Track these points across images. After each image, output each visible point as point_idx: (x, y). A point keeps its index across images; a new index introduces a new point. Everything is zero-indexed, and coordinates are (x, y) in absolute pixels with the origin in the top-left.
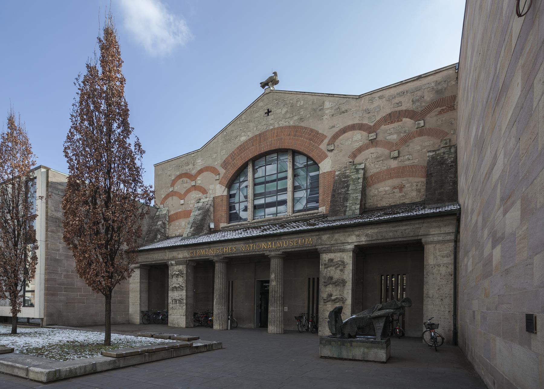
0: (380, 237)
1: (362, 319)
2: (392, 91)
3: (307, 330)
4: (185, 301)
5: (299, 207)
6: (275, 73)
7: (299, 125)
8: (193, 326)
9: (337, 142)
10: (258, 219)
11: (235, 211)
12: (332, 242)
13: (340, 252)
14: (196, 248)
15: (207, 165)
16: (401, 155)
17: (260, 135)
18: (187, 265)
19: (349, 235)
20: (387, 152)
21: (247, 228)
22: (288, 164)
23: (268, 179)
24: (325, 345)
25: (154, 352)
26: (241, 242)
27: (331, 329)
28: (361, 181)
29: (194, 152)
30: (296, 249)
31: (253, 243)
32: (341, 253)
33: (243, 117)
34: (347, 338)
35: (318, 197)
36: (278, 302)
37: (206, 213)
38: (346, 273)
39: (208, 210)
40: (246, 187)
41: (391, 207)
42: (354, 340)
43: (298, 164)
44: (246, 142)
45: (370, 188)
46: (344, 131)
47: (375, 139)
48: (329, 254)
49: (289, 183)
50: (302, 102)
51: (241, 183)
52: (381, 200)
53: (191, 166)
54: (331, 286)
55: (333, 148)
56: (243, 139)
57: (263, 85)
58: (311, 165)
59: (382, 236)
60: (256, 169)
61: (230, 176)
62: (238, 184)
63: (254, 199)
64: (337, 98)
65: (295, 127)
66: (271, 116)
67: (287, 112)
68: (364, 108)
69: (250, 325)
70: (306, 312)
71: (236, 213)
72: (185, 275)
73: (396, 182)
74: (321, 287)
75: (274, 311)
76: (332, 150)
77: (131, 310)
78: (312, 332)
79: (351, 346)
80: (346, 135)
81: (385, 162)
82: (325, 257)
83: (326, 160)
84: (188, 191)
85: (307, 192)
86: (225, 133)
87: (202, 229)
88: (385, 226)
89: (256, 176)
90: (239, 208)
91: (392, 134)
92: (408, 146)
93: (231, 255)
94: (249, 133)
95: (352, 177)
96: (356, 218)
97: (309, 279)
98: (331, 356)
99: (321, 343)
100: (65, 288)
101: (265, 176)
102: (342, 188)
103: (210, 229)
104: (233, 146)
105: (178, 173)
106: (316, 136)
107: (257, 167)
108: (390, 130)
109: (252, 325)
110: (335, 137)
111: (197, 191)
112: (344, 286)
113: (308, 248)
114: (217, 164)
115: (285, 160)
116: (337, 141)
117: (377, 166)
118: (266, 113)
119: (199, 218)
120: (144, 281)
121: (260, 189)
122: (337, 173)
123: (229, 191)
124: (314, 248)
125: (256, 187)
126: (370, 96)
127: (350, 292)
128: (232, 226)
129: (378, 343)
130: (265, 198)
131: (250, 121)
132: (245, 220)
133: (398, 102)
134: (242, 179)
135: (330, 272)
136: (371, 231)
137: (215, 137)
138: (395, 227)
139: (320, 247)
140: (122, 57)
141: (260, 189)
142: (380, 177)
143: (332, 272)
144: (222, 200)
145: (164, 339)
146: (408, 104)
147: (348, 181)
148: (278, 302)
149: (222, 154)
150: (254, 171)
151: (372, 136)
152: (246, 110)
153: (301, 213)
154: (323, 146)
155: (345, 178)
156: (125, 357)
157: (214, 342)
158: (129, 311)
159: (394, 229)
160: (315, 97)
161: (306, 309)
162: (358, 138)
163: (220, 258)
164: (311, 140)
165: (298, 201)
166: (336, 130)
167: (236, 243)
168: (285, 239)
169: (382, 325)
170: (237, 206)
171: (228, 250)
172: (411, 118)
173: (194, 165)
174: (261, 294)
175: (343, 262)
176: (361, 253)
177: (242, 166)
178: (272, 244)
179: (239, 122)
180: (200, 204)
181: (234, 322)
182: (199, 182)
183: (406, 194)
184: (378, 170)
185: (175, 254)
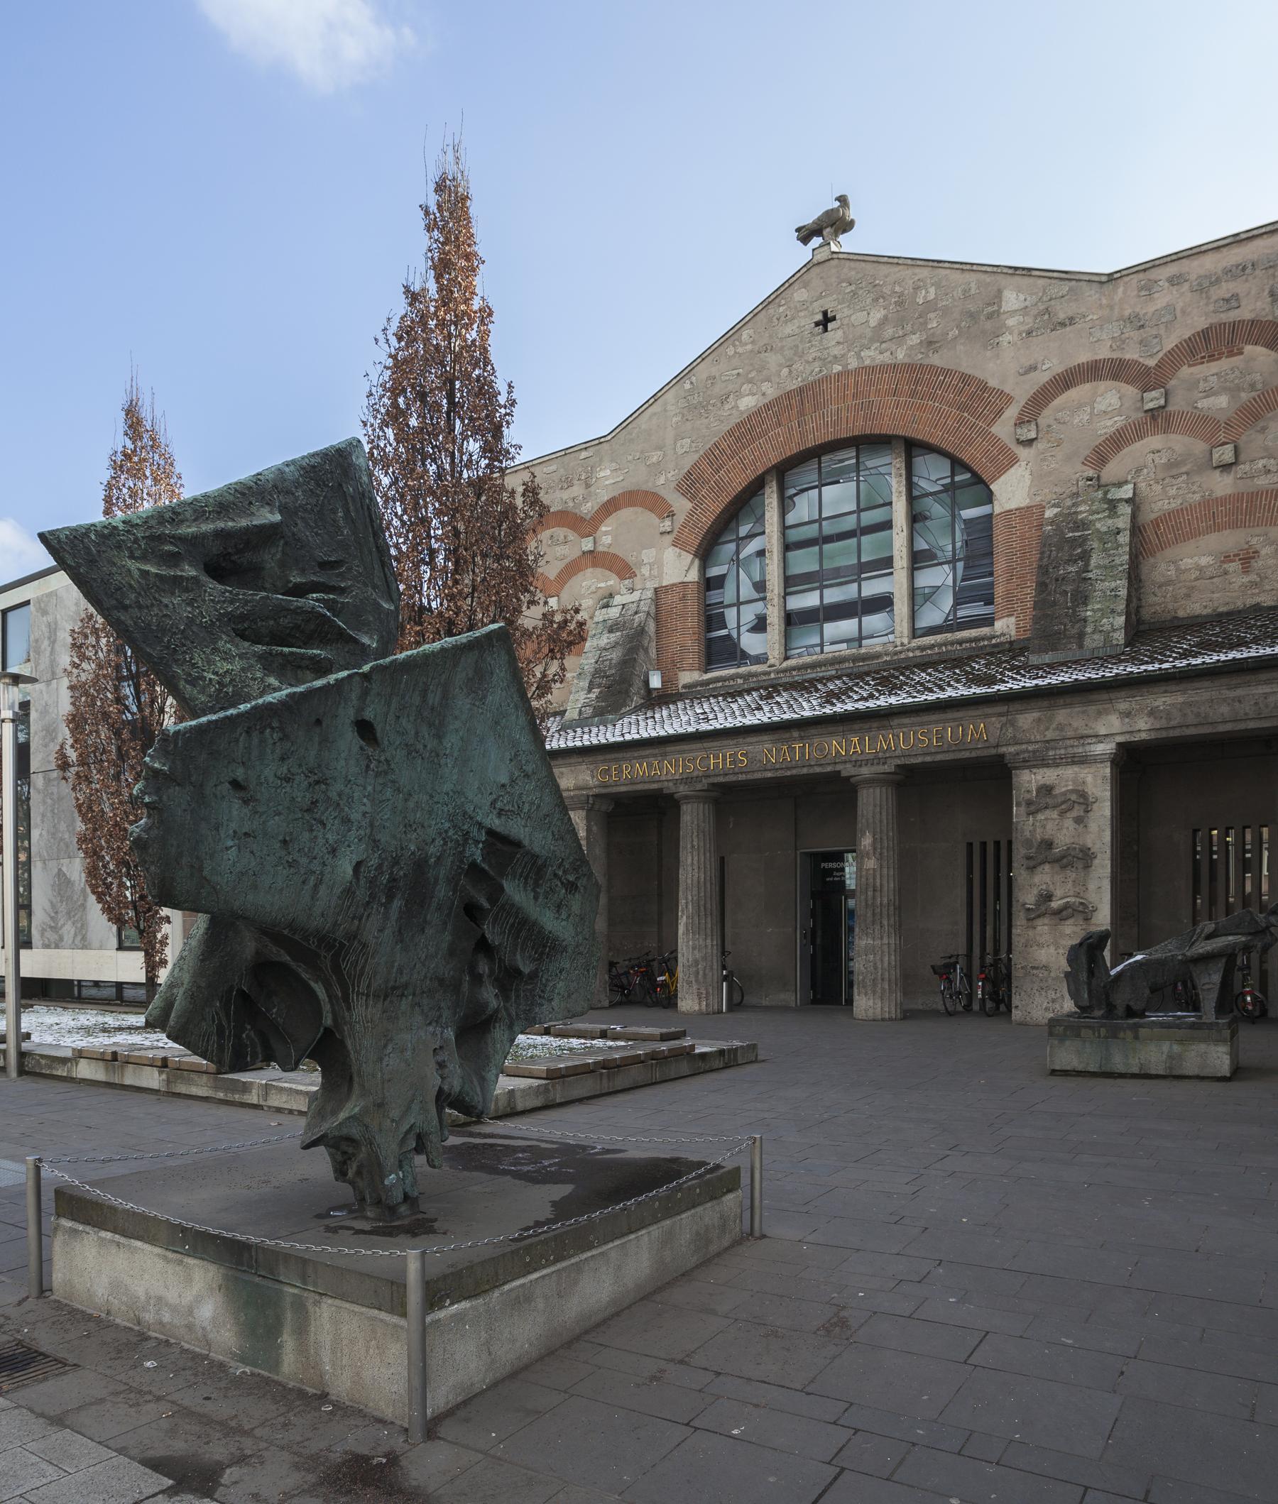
0: (1191, 719)
1: (1161, 963)
2: (1209, 264)
3: (968, 1008)
5: (932, 616)
6: (843, 200)
7: (925, 362)
8: (606, 1003)
10: (800, 655)
11: (723, 632)
12: (1050, 735)
13: (1074, 763)
14: (620, 755)
15: (628, 485)
16: (1242, 457)
17: (801, 390)
18: (589, 811)
19: (1099, 713)
20: (1199, 447)
21: (771, 689)
22: (894, 482)
23: (828, 528)
24: (1062, 1038)
25: (618, 1066)
26: (766, 738)
27: (1074, 995)
28: (1124, 538)
29: (586, 446)
30: (939, 758)
31: (802, 738)
32: (1076, 769)
33: (745, 335)
34: (1122, 1018)
35: (991, 585)
36: (885, 923)
37: (634, 641)
38: (1093, 826)
39: (641, 631)
40: (761, 553)
41: (1219, 618)
42: (1142, 1021)
43: (923, 483)
44: (758, 412)
45: (1152, 560)
46: (1066, 381)
47: (1163, 407)
49: (899, 540)
50: (932, 290)
51: (741, 541)
52: (1188, 596)
53: (577, 490)
54: (1047, 867)
55: (1033, 435)
56: (748, 403)
57: (805, 235)
58: (963, 485)
59: (1198, 715)
60: (791, 497)
61: (707, 520)
62: (732, 546)
63: (786, 594)
64: (1041, 282)
65: (910, 368)
66: (835, 333)
67: (884, 322)
68: (1127, 313)
69: (782, 996)
70: (962, 950)
71: (729, 637)
73: (1230, 540)
74: (1019, 873)
75: (870, 952)
76: (1030, 442)
78: (995, 1013)
79: (1136, 1038)
80: (1073, 394)
81: (1196, 478)
82: (1028, 781)
83: (1012, 470)
85: (954, 569)
86: (687, 386)
87: (627, 692)
88: (1207, 684)
89: (791, 519)
90: (737, 621)
91: (1214, 394)
92: (1264, 429)
94: (766, 387)
95: (1098, 525)
96: (1117, 659)
97: (970, 845)
98: (1080, 1067)
99: (1051, 1034)
101: (820, 520)
102: (1068, 562)
103: (649, 691)
104: (716, 426)
106: (979, 398)
107: (792, 491)
108: (1205, 380)
109: (790, 998)
111: (599, 570)
112: (1087, 867)
113: (974, 754)
114: (665, 483)
115: (882, 470)
116: (1047, 412)
117: (1172, 492)
118: (817, 324)
119: (615, 655)
121: (805, 562)
122: (1049, 513)
123: (703, 568)
124: (993, 751)
125: (790, 554)
126: (1141, 276)
127: (1106, 885)
129: (1210, 1026)
130: (822, 588)
131: (768, 348)
133: (1227, 296)
134: (744, 530)
135: (1044, 827)
136: (1163, 700)
137: (655, 397)
138: (1236, 687)
139: (1012, 749)
140: (480, 249)
141: (805, 562)
142: (1184, 525)
143: (1050, 826)
144: (684, 598)
145: (585, 1038)
146: (1259, 304)
147: (1085, 539)
148: (885, 923)
149: (685, 452)
151: (1154, 399)
152: (754, 314)
153: (939, 638)
154: (1003, 429)
156: (564, 1076)
157: (737, 1043)
159: (1232, 694)
160: (972, 278)
161: (963, 940)
162: (1109, 404)
163: (699, 787)
164: (962, 408)
166: (1042, 377)
167: (749, 740)
168: (905, 726)
169: (1217, 978)
170: (731, 614)
171: (721, 761)
172: (1269, 346)
173: (588, 486)
174: (814, 895)
175: (1083, 795)
176: (1133, 763)
177: (744, 491)
178: (861, 741)
179: (731, 351)
180: (614, 612)
181: (740, 991)
182: (607, 540)
183: (1263, 578)
184: (1175, 504)
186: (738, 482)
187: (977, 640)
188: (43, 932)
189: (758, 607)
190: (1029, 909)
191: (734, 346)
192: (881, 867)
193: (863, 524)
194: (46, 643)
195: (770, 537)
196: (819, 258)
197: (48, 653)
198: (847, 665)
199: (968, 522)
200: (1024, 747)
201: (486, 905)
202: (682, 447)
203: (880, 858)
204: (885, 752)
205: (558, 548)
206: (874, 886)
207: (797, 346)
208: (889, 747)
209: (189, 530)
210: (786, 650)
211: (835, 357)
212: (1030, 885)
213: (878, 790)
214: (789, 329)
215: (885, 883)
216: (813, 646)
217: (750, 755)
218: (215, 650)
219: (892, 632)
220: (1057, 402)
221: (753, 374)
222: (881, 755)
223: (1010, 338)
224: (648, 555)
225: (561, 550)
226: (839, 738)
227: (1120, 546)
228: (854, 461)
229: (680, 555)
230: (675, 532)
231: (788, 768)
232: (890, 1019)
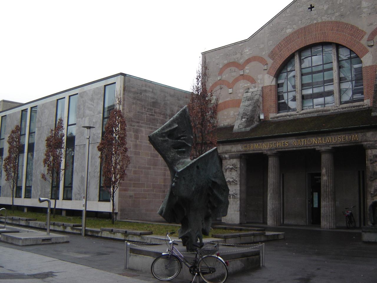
4: (239, 196)
5: (346, 97)
7: (341, 21)
10: (306, 109)
11: (283, 101)
17: (305, 28)
23: (314, 69)
26: (293, 138)
30: (344, 145)
35: (362, 89)
36: (330, 197)
40: (294, 76)
43: (341, 56)
44: (292, 34)
53: (238, 55)
56: (289, 31)
58: (354, 58)
61: (278, 66)
62: (285, 74)
63: (302, 89)
65: (336, 22)
72: (238, 169)
83: (367, 55)
84: (236, 80)
85: (352, 83)
86: (271, 25)
87: (253, 121)
89: (303, 66)
90: (287, 98)
93: (284, 150)
94: (294, 26)
101: (312, 67)
103: (260, 120)
105: (226, 62)
106: (357, 32)
107: (303, 58)
111: (245, 81)
114: (265, 54)
115: (330, 52)
118: (309, 8)
119: (250, 108)
121: (307, 79)
123: (277, 80)
125: (303, 77)
128: (281, 116)
130: (313, 88)
132: (294, 110)
139: (365, 143)
141: (307, 79)
148: (330, 197)
150: (301, 62)
154: (364, 41)
165: (345, 92)
170: (285, 95)
173: (242, 54)
178: (322, 139)
179: (284, 15)
180: (249, 94)
185: (228, 148)
186: (287, 55)
187: (359, 106)
188: (75, 195)
189: (293, 93)
190: (372, 194)
191: (285, 14)
192: (328, 179)
194: (82, 106)
195: (297, 72)
197: (82, 109)
198: (320, 113)
199: (355, 69)
200: (368, 142)
201: (211, 194)
202: (270, 43)
203: (328, 176)
204: (328, 143)
205: (232, 73)
206: (326, 186)
207: (303, 15)
208: (330, 141)
209: (166, 131)
210: (302, 107)
211: (314, 18)
213: (327, 155)
214: (300, 10)
215: (330, 184)
216: (310, 106)
217: (289, 143)
218: (171, 152)
219: (334, 103)
222: (327, 144)
223: (364, 15)
224: (260, 77)
226: (315, 138)
228: (321, 49)
229: (269, 77)
230: (268, 70)
231: (300, 147)
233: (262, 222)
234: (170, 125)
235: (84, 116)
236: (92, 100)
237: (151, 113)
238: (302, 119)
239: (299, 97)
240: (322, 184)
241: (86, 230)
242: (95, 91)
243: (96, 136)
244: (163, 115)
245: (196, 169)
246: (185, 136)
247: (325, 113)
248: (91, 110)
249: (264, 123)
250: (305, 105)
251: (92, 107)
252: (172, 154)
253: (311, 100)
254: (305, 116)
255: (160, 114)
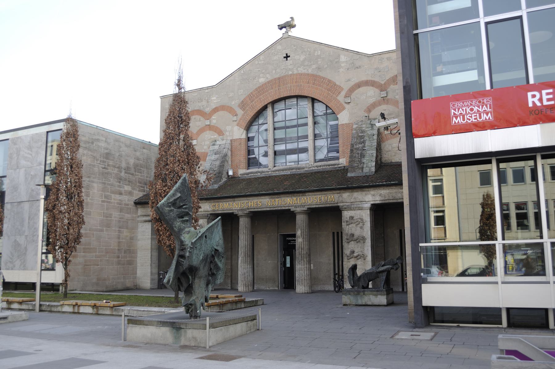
0: (391, 198)
5: (321, 155)
6: (292, 18)
7: (317, 74)
9: (353, 95)
11: (253, 156)
17: (279, 78)
23: (288, 124)
27: (350, 283)
28: (375, 137)
29: (208, 88)
30: (320, 206)
32: (360, 211)
33: (261, 57)
38: (365, 230)
39: (226, 155)
40: (266, 130)
44: (265, 84)
46: (359, 85)
48: (350, 212)
50: (319, 52)
53: (204, 103)
54: (352, 242)
56: (262, 80)
57: (281, 27)
59: (393, 196)
61: (249, 118)
62: (257, 127)
65: (313, 75)
67: (305, 59)
74: (345, 244)
77: (139, 272)
80: (361, 89)
82: (346, 214)
85: (327, 141)
86: (242, 72)
90: (258, 153)
94: (268, 76)
100: (84, 248)
101: (285, 121)
102: (359, 143)
103: (228, 176)
106: (334, 88)
110: (352, 90)
111: (211, 132)
113: (331, 205)
114: (234, 104)
115: (305, 106)
118: (284, 57)
119: (218, 163)
120: (155, 237)
121: (280, 134)
122: (355, 126)
123: (247, 133)
124: (336, 205)
125: (275, 131)
128: (251, 173)
130: (286, 143)
132: (266, 166)
134: (261, 121)
141: (280, 134)
143: (353, 229)
144: (240, 144)
151: (384, 94)
154: (341, 98)
155: (362, 132)
158: (136, 274)
161: (332, 266)
164: (329, 90)
166: (352, 83)
170: (256, 150)
173: (208, 102)
175: (362, 220)
177: (261, 109)
180: (216, 147)
182: (214, 121)
187: (334, 165)
188: (6, 264)
189: (265, 148)
193: (299, 123)
194: (15, 155)
196: (285, 36)
198: (294, 171)
209: (171, 201)
212: (348, 248)
220: (356, 91)
221: (264, 71)
224: (228, 128)
225: (199, 123)
227: (374, 140)
232: (307, 293)
233: (230, 288)
234: (174, 195)
235: (18, 167)
236: (30, 148)
237: (103, 166)
238: (275, 176)
239: (271, 153)
240: (297, 246)
241: (40, 305)
242: (33, 138)
243: (35, 193)
244: (117, 168)
245: (204, 238)
246: (187, 205)
247: (299, 172)
248: (28, 161)
249: (232, 179)
250: (277, 162)
251: (30, 156)
252: (178, 224)
253: (284, 156)
254: (277, 173)
255: (114, 167)
